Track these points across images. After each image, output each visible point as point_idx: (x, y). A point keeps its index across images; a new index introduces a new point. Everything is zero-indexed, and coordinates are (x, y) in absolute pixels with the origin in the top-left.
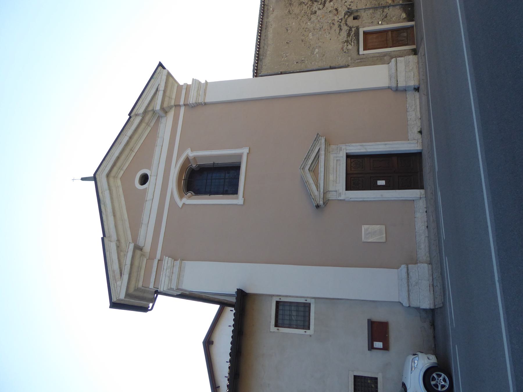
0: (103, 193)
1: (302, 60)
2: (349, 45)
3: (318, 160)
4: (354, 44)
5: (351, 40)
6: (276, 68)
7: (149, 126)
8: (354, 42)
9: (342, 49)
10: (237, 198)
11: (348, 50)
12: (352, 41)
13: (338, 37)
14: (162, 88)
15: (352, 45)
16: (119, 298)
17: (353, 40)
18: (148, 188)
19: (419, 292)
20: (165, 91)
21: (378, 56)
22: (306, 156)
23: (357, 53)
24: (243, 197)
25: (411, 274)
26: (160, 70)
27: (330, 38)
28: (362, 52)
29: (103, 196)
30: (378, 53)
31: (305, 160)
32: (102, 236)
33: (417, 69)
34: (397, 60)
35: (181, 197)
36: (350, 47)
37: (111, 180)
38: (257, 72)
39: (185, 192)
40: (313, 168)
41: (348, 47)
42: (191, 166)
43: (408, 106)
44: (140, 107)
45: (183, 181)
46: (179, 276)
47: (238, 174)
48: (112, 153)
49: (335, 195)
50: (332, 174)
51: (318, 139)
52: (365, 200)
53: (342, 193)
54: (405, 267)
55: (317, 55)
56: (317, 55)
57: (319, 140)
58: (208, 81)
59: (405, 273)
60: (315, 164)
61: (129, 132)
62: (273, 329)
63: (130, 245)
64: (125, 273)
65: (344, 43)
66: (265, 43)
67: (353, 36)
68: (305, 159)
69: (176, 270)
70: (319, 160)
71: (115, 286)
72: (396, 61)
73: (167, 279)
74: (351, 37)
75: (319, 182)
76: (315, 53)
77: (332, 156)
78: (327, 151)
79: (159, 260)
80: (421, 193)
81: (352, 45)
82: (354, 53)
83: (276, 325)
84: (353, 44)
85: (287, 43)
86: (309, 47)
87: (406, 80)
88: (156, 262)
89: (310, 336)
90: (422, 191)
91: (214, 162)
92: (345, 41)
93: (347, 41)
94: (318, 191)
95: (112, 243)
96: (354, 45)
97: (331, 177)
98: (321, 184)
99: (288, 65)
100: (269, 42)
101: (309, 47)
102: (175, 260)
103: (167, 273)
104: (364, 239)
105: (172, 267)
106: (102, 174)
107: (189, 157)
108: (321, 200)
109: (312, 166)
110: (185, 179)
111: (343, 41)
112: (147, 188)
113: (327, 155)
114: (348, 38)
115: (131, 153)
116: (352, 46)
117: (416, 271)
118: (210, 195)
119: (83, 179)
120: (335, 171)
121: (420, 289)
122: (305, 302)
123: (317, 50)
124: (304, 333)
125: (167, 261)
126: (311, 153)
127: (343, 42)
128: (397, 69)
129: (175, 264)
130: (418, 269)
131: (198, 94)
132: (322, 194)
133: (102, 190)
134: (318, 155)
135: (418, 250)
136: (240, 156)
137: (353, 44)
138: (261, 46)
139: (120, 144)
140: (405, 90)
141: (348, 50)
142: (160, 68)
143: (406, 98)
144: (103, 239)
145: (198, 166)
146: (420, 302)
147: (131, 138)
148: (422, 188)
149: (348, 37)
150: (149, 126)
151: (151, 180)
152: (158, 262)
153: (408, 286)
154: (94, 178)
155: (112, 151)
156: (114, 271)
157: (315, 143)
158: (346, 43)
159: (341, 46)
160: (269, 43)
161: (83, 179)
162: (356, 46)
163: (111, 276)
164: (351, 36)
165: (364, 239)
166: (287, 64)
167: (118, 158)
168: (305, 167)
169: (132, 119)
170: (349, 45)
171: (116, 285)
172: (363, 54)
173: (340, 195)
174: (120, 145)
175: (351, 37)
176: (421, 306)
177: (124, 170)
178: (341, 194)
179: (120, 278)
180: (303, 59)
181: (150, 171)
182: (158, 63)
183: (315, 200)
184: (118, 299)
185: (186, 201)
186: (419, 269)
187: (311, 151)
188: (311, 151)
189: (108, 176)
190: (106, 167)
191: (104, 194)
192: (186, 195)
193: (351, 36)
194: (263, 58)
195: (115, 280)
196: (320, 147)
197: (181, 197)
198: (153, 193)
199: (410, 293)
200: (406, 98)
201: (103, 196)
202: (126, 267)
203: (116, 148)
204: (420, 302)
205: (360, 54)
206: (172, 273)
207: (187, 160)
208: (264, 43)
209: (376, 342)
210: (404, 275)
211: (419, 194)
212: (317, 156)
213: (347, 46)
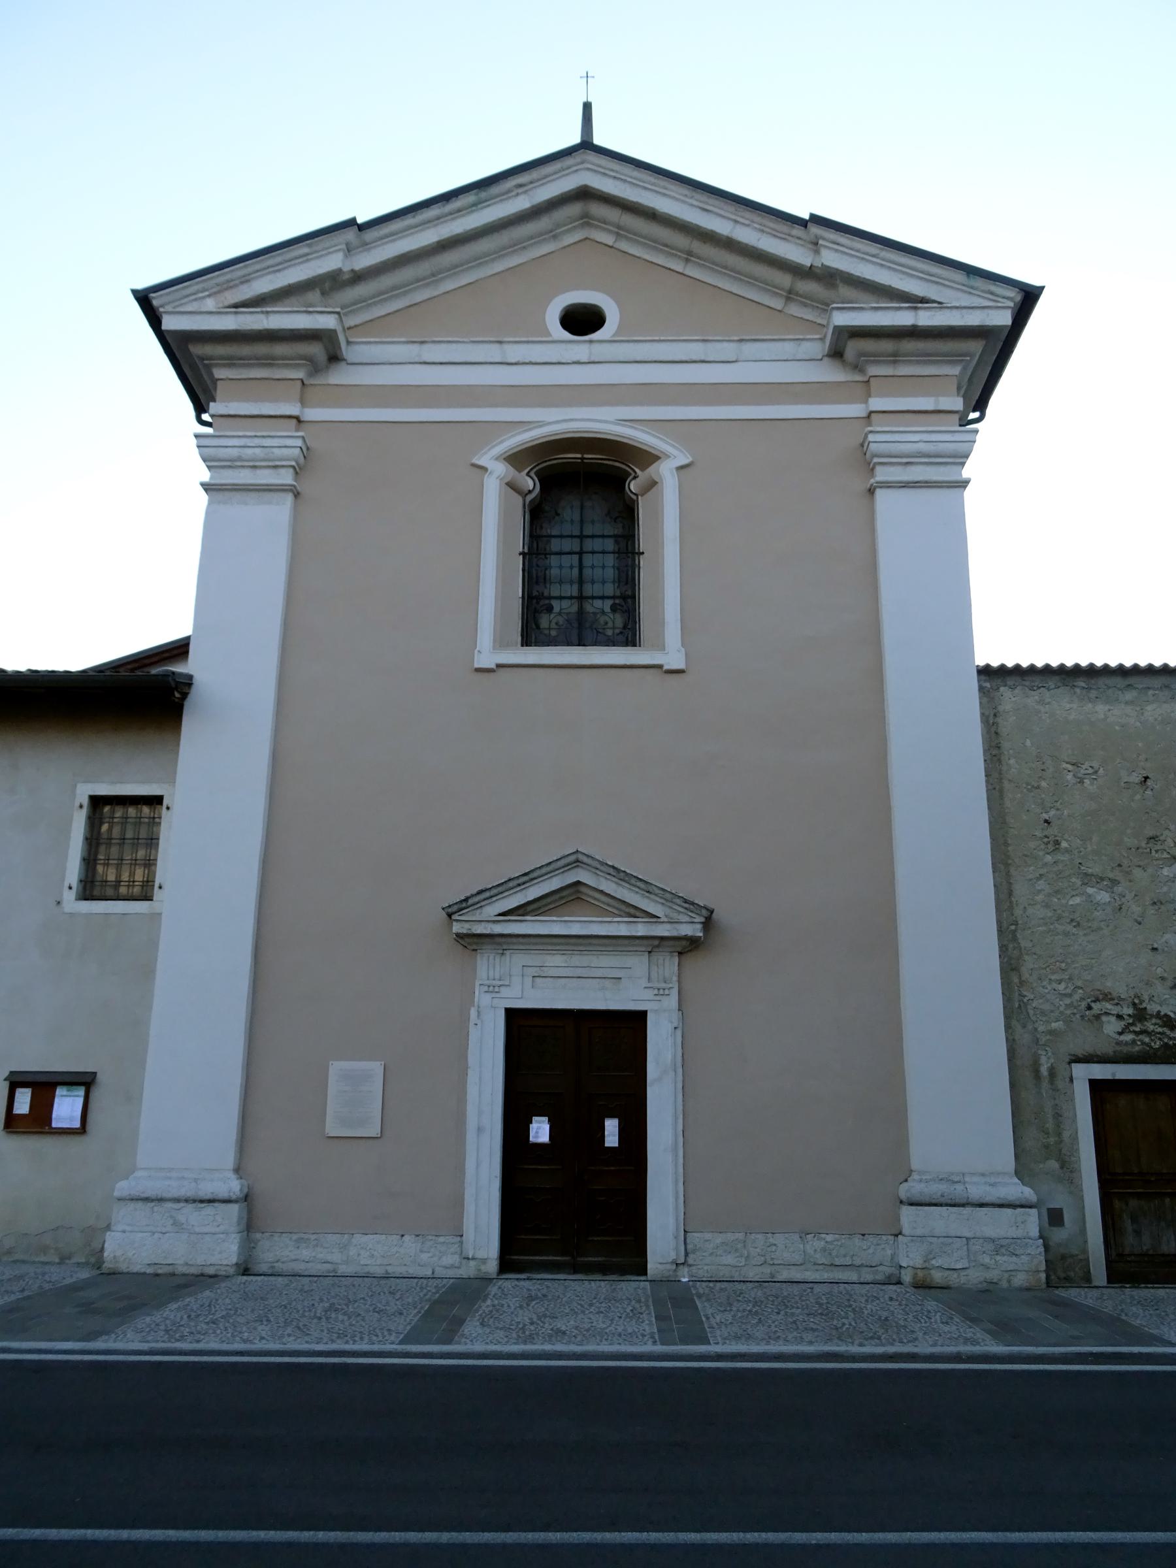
0: (520, 190)
1: (1057, 843)
2: (1123, 1023)
3: (622, 913)
4: (1127, 1044)
5: (1142, 1032)
6: (1028, 743)
7: (788, 299)
8: (1134, 1042)
9: (1107, 997)
10: (500, 643)
11: (1097, 1017)
12: (1141, 1037)
13: (1163, 978)
14: (926, 318)
15: (1120, 1034)
16: (165, 312)
17: (1147, 1040)
18: (550, 339)
19: (154, 1233)
20: (913, 333)
21: (1059, 1135)
22: (624, 872)
23: (1080, 1052)
24: (499, 666)
25: (209, 1210)
26: (1004, 298)
27: (1160, 947)
28: (1083, 1073)
29: (509, 191)
30: (1075, 1138)
31: (609, 868)
32: (360, 221)
33: (981, 1283)
34: (1030, 1207)
35: (516, 459)
36: (1111, 1026)
37: (575, 209)
38: (986, 672)
39: (537, 468)
40: (595, 899)
41: (1113, 1019)
42: (633, 474)
43: (829, 1238)
44: (853, 253)
45: (579, 456)
46: (220, 490)
47: (611, 642)
48: (666, 189)
49: (491, 973)
50: (566, 961)
51: (692, 912)
52: (680, 1085)
53: (498, 995)
54: (232, 1194)
55: (1077, 900)
56: (1077, 900)
57: (690, 914)
58: (968, 493)
59: (212, 1193)
60: (603, 903)
61: (747, 235)
62: (85, 791)
63: (333, 315)
64: (241, 318)
65: (1134, 1004)
66: (1151, 692)
67: (1166, 1040)
68: (613, 867)
69: (265, 477)
70: (620, 916)
71: (201, 295)
72: (1022, 1206)
73: (234, 453)
74: (1160, 1030)
75: (528, 918)
76: (1090, 890)
77: (637, 963)
78: (655, 944)
79: (298, 419)
80: (484, 1261)
81: (1120, 1034)
82: (1086, 1042)
83: (97, 802)
84: (1128, 1037)
85: (1146, 778)
86: (1120, 865)
87: (930, 1239)
88: (292, 409)
89: (59, 902)
90: (492, 1266)
91: (643, 553)
92: (1141, 1007)
93: (1141, 1015)
94: (500, 915)
95: (340, 255)
96: (1118, 1043)
97: (555, 961)
98: (523, 924)
99: (1038, 787)
100: (1155, 706)
101: (1120, 865)
102: (298, 471)
103: (249, 451)
104: (336, 1067)
105: (271, 464)
106: (588, 169)
107: (659, 461)
108: (467, 926)
109: (597, 895)
110: (585, 461)
111: (1141, 1002)
112: (551, 335)
113: (641, 945)
114: (1158, 1021)
115: (680, 257)
116: (1117, 1037)
117: (218, 1226)
118: (523, 554)
119: (587, 107)
120: (579, 972)
121: (161, 1235)
122: (157, 885)
123: (1104, 897)
124: (66, 885)
125: (287, 444)
126: (639, 888)
127: (1136, 1001)
128: (982, 1205)
129: (283, 471)
130: (223, 1233)
131: (908, 460)
132: (485, 928)
133: (531, 183)
134: (638, 914)
135: (295, 1237)
136: (661, 647)
137: (1128, 1037)
138: (1132, 680)
139: (700, 208)
140: (900, 1233)
141: (1097, 1017)
142: (1016, 296)
143: (863, 1235)
144: (351, 222)
145: (633, 501)
146: (124, 1232)
147: (729, 244)
148: (507, 1264)
149: (1160, 1019)
150: (788, 299)
151: (579, 347)
152: (290, 417)
153: (177, 1200)
154: (587, 144)
155: (672, 187)
156: (248, 281)
157: (674, 900)
158: (1130, 1011)
159: (1120, 990)
160: (1149, 708)
161: (587, 107)
162: (1114, 1052)
163: (229, 277)
164: (1165, 1030)
165: (336, 1067)
166: (1044, 784)
167: (651, 215)
168: (588, 867)
169: (798, 231)
170: (1123, 1023)
171: (204, 298)
172: (1071, 1080)
173: (492, 989)
174: (698, 210)
175: (1160, 1030)
176: (113, 1233)
177: (617, 245)
178: (494, 995)
179: (227, 304)
180: (1064, 844)
181: (614, 335)
182: (1036, 282)
183: (464, 905)
184: (161, 310)
185: (499, 470)
186: (221, 1236)
187: (647, 888)
188: (647, 888)
189: (584, 194)
190: (615, 177)
191: (518, 194)
192: (528, 474)
193: (1168, 1032)
194: (1078, 690)
195: (219, 292)
196: (664, 919)
197: (516, 459)
198: (527, 361)
199: (153, 1204)
200: (863, 1235)
201: (509, 191)
202: (262, 316)
203: (686, 196)
204: (124, 1232)
205: (1073, 1064)
206: (255, 467)
207: (647, 458)
208: (1149, 688)
209: (30, 1094)
210: (208, 1189)
211: (481, 1254)
212: (632, 911)
213: (1120, 1017)
